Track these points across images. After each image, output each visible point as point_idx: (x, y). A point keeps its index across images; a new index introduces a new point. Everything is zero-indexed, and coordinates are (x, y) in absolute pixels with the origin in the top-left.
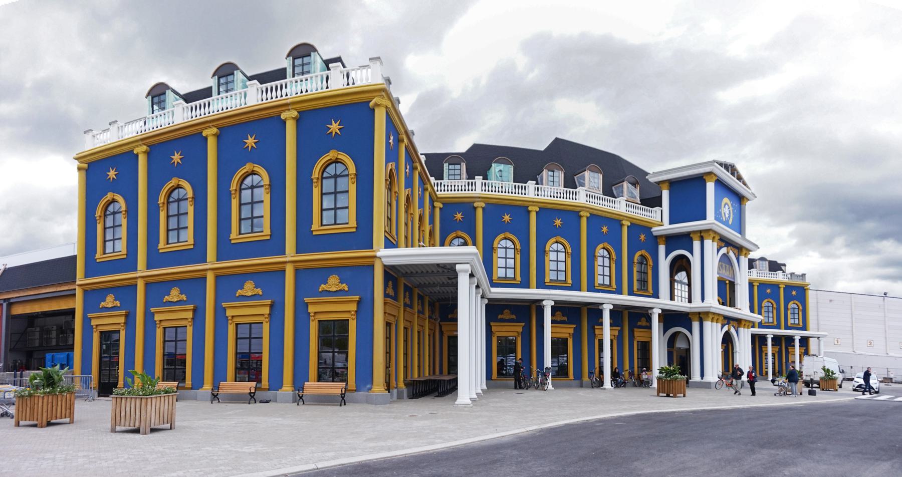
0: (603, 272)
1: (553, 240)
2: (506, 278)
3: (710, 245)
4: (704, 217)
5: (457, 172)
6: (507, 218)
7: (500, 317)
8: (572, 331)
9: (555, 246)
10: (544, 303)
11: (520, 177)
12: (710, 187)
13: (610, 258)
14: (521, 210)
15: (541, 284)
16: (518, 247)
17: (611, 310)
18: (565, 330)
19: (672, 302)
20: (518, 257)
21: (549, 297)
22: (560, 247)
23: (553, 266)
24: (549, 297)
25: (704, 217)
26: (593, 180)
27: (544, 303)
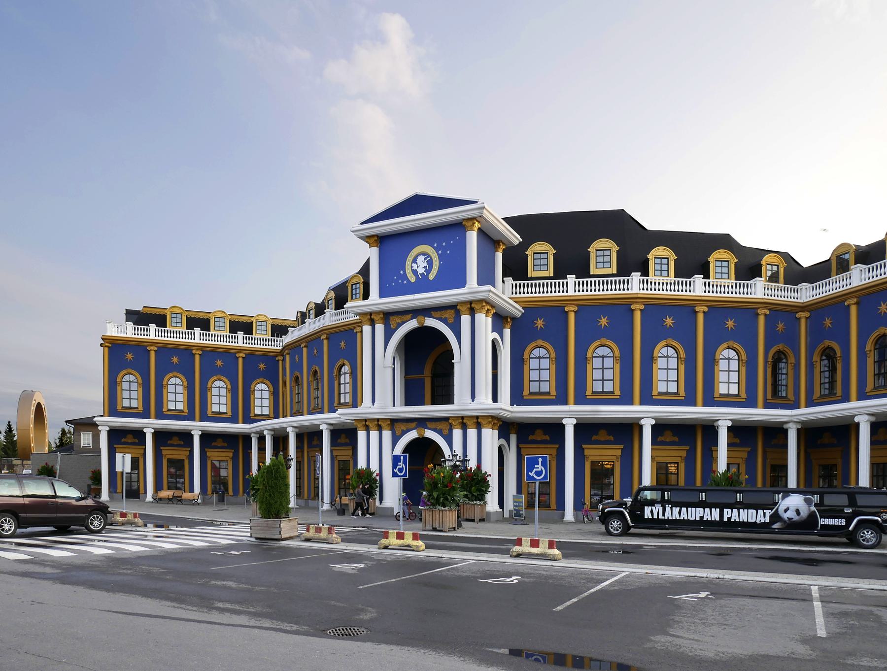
0: (728, 376)
1: (664, 343)
2: (667, 393)
3: (484, 321)
4: (462, 284)
5: (544, 262)
6: (669, 321)
7: (123, 440)
8: (684, 454)
9: (664, 351)
10: (720, 423)
11: (684, 270)
12: (472, 237)
13: (739, 360)
14: (685, 309)
15: (710, 400)
16: (683, 355)
17: (575, 426)
18: (180, 453)
19: (495, 405)
20: (682, 368)
21: (647, 415)
22: (671, 352)
23: (597, 375)
24: (647, 415)
25: (462, 284)
26: (603, 253)
27: (720, 423)
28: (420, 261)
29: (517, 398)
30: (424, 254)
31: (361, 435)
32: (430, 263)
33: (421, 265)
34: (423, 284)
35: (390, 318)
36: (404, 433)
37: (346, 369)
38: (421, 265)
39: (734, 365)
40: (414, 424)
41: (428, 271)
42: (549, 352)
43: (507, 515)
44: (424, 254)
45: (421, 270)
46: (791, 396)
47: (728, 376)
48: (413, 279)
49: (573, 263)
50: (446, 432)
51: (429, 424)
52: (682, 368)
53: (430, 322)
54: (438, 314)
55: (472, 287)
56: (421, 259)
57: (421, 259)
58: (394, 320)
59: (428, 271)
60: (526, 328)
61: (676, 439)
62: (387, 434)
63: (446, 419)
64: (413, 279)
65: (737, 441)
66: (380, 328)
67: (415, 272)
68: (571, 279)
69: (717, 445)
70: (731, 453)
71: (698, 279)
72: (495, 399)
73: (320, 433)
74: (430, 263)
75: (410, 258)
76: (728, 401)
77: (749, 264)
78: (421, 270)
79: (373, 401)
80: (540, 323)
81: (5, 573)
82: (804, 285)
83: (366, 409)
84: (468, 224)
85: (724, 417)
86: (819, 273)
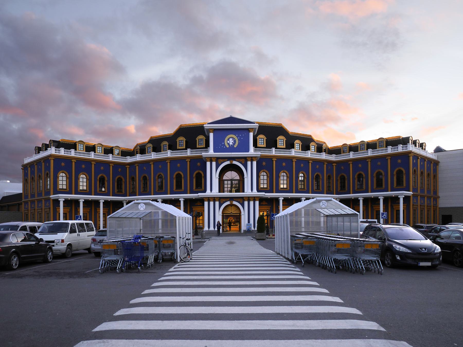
0: (83, 184)
6: (284, 164)
16: (288, 175)
27: (280, 198)
28: (230, 141)
29: (258, 190)
30: (232, 138)
31: (206, 203)
32: (235, 141)
33: (231, 142)
34: (231, 149)
35: (219, 160)
36: (224, 202)
37: (49, 180)
38: (231, 142)
39: (285, 178)
40: (229, 199)
41: (234, 144)
42: (286, 174)
43: (242, 232)
44: (232, 138)
45: (231, 144)
46: (123, 192)
47: (83, 184)
48: (228, 146)
49: (271, 144)
50: (241, 202)
51: (235, 199)
52: (288, 180)
53: (235, 162)
54: (238, 160)
55: (252, 151)
56: (231, 139)
57: (231, 139)
58: (220, 161)
59: (234, 144)
60: (264, 164)
61: (267, 203)
62: (217, 203)
63: (242, 198)
64: (228, 146)
65: (66, 205)
66: (214, 164)
67: (229, 144)
68: (189, 150)
69: (79, 207)
70: (65, 210)
71: (92, 153)
72: (252, 190)
73: (359, 201)
74: (235, 141)
75: (226, 139)
76: (283, 191)
77: (320, 148)
78: (231, 144)
79: (211, 190)
80: (264, 163)
81: (27, 275)
82: (129, 157)
83: (208, 193)
84: (251, 130)
85: (82, 198)
86: (331, 151)
